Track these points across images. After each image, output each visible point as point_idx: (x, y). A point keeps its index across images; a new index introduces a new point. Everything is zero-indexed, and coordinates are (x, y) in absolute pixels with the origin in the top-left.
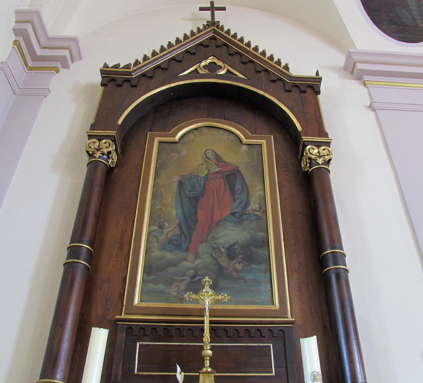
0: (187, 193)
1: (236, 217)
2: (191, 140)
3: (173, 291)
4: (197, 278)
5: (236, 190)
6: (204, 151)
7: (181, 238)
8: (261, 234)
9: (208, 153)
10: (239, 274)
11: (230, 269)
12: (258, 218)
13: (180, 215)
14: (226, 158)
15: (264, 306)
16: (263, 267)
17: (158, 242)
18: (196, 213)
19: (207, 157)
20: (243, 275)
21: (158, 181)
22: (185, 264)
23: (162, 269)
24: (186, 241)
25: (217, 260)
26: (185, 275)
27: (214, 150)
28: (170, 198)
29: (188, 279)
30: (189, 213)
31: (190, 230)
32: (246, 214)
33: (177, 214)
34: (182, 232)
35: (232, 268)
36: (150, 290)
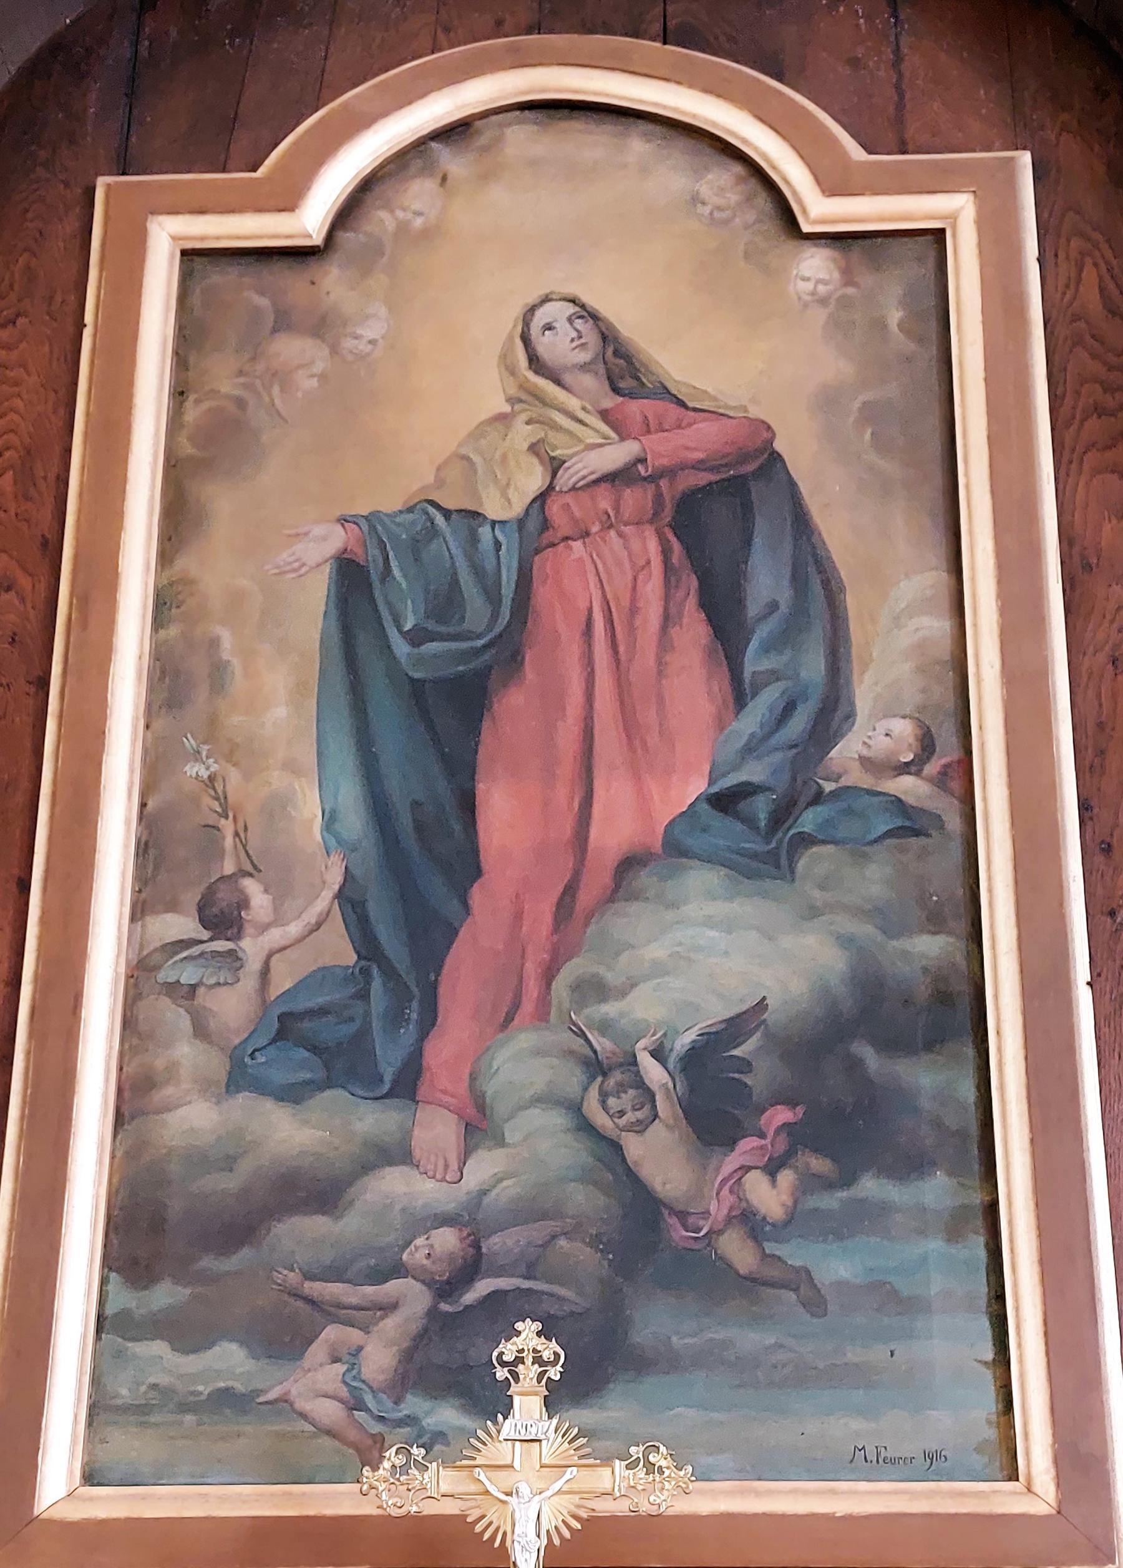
0: (401, 648)
1: (749, 822)
2: (418, 222)
3: (314, 1385)
4: (483, 1287)
5: (753, 609)
6: (516, 310)
7: (364, 995)
8: (932, 946)
9: (549, 327)
10: (770, 1247)
11: (706, 1214)
12: (911, 824)
13: (355, 822)
14: (677, 359)
15: (945, 1485)
16: (937, 1190)
17: (201, 1031)
18: (468, 805)
19: (535, 362)
20: (794, 1253)
21: (186, 563)
22: (394, 1184)
23: (238, 1227)
24: (396, 1018)
25: (617, 1147)
26: (398, 1270)
27: (586, 298)
28: (280, 699)
29: (413, 1298)
30: (416, 805)
31: (432, 935)
32: (818, 798)
33: (330, 820)
34: (368, 946)
35: (718, 1208)
36: (154, 1387)
